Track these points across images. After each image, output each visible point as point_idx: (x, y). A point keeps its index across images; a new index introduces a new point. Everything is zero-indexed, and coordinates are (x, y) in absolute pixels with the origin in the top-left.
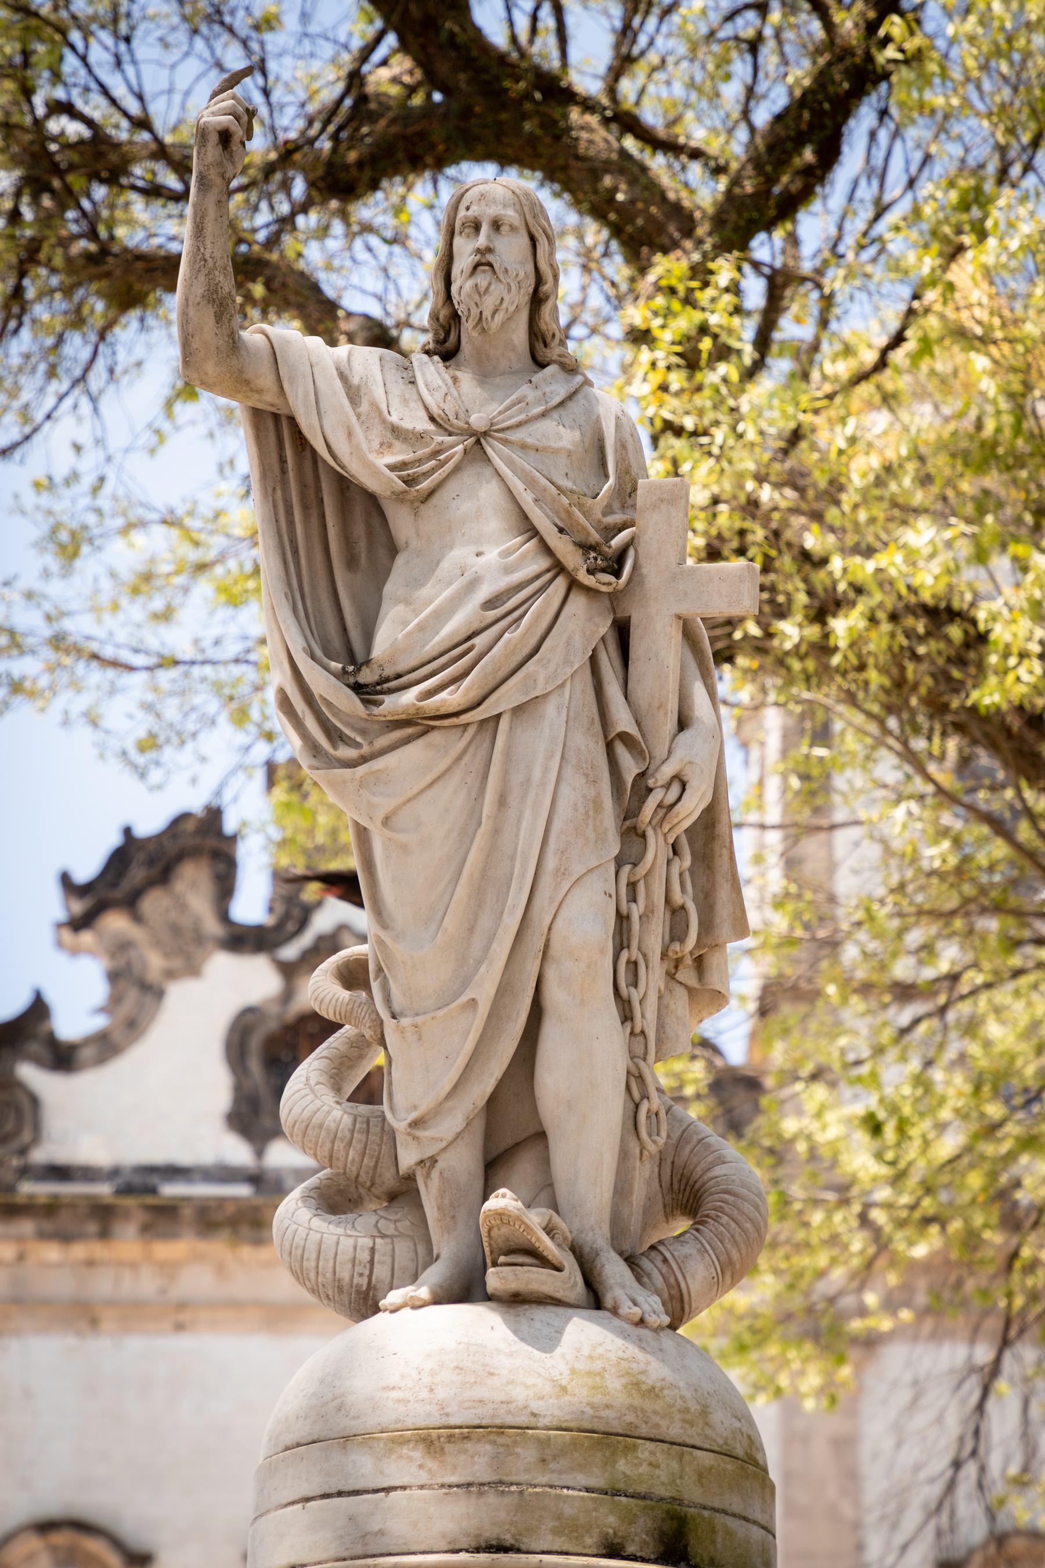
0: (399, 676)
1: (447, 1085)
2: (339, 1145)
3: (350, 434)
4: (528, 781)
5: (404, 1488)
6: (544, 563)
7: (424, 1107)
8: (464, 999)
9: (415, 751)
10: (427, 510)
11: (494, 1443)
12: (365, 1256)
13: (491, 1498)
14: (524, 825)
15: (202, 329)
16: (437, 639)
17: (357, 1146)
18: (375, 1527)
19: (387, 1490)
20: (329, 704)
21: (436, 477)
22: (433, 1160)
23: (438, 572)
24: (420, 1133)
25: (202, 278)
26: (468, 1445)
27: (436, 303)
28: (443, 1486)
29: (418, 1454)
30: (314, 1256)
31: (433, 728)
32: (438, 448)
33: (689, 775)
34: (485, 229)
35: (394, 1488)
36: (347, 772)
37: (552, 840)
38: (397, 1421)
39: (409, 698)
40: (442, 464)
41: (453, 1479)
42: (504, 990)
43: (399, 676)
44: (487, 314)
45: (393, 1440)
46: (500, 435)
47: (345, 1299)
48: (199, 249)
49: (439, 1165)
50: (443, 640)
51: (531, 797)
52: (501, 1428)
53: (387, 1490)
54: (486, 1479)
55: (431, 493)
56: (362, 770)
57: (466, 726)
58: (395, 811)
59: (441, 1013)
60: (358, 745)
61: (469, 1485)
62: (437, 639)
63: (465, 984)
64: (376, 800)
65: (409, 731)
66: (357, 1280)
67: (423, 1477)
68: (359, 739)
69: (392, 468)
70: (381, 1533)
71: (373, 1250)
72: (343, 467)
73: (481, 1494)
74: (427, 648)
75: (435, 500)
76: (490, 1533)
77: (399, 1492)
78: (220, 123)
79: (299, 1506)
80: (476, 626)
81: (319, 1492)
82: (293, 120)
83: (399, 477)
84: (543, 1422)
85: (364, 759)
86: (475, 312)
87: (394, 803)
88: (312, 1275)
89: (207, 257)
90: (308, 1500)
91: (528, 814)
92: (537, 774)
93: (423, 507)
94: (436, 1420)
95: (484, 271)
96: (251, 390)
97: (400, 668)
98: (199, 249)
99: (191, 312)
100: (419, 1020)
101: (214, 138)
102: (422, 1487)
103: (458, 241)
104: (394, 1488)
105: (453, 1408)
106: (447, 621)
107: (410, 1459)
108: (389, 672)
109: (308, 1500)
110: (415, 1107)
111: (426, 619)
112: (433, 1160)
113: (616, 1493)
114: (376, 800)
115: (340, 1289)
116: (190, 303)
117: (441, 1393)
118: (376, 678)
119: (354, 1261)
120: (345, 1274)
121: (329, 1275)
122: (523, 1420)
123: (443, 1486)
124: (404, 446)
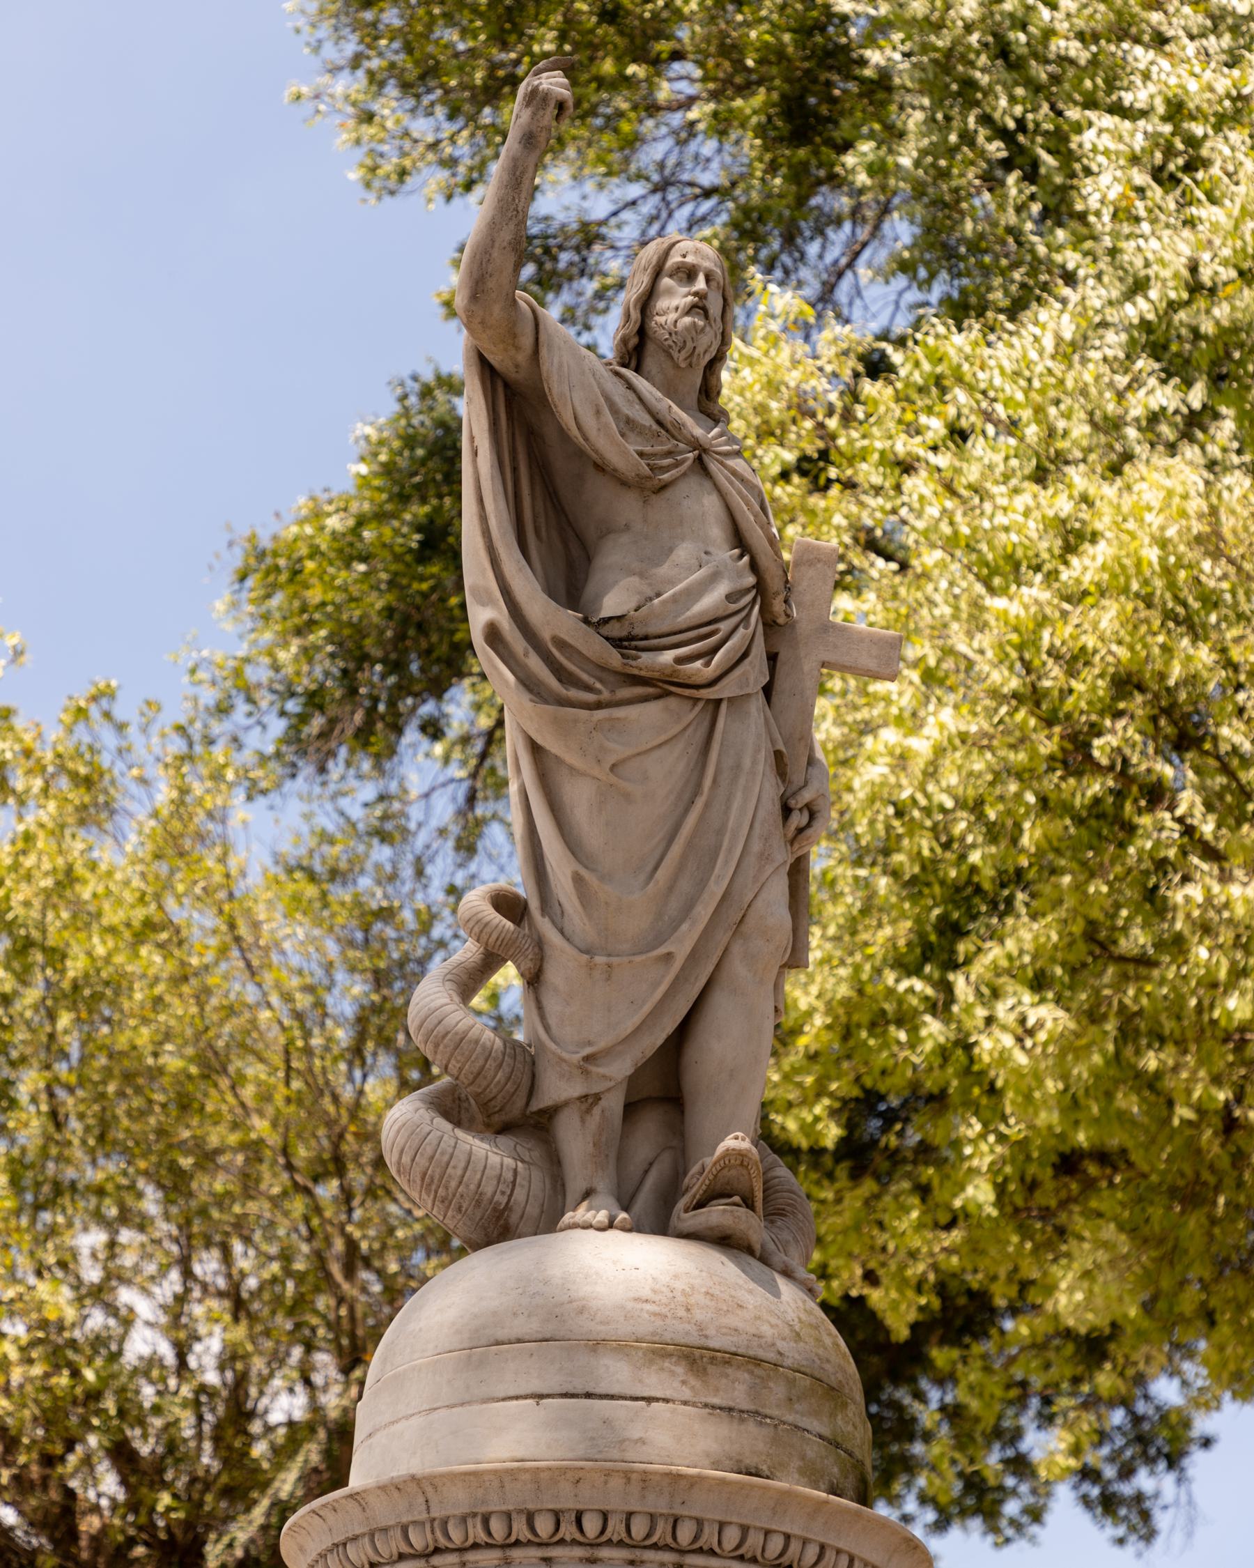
0: (646, 638)
2: (491, 1064)
3: (598, 412)
4: (738, 767)
6: (750, 580)
7: (602, 1044)
8: (662, 950)
9: (652, 712)
10: (658, 501)
11: (751, 1373)
12: (509, 1176)
13: (751, 1426)
14: (736, 805)
17: (506, 1068)
18: (636, 1434)
19: (649, 1400)
20: (561, 644)
22: (597, 1097)
23: (673, 557)
25: (512, 226)
26: (729, 1371)
28: (706, 1406)
31: (670, 694)
35: (657, 1400)
36: (583, 713)
37: (757, 825)
39: (668, 657)
40: (677, 464)
41: (716, 1401)
42: (694, 956)
43: (646, 638)
44: (700, 350)
45: (654, 1352)
47: (478, 1214)
49: (603, 1103)
51: (742, 781)
52: (757, 1361)
53: (649, 1400)
54: (745, 1407)
55: (664, 487)
56: (600, 714)
57: (698, 700)
59: (638, 959)
60: (598, 692)
61: (730, 1409)
63: (660, 940)
64: (611, 745)
65: (650, 690)
66: (498, 1197)
67: (686, 1394)
68: (598, 685)
69: (641, 454)
70: (642, 1441)
71: (515, 1171)
72: (586, 439)
73: (742, 1420)
75: (668, 494)
76: (750, 1461)
77: (661, 1405)
80: (721, 613)
81: (557, 1390)
82: (755, 112)
84: (788, 1362)
85: (599, 706)
86: (690, 345)
87: (629, 752)
88: (453, 1184)
90: (540, 1396)
91: (739, 797)
92: (747, 762)
94: (695, 1339)
97: (653, 629)
101: (552, 104)
102: (685, 1403)
103: (666, 282)
104: (657, 1400)
105: (711, 1332)
106: (696, 601)
107: (673, 1373)
108: (639, 631)
109: (540, 1396)
110: (590, 1043)
111: (681, 593)
112: (597, 1097)
113: (838, 1446)
114: (611, 745)
117: (699, 1315)
118: (624, 633)
120: (488, 1189)
122: (771, 1356)
123: (706, 1406)
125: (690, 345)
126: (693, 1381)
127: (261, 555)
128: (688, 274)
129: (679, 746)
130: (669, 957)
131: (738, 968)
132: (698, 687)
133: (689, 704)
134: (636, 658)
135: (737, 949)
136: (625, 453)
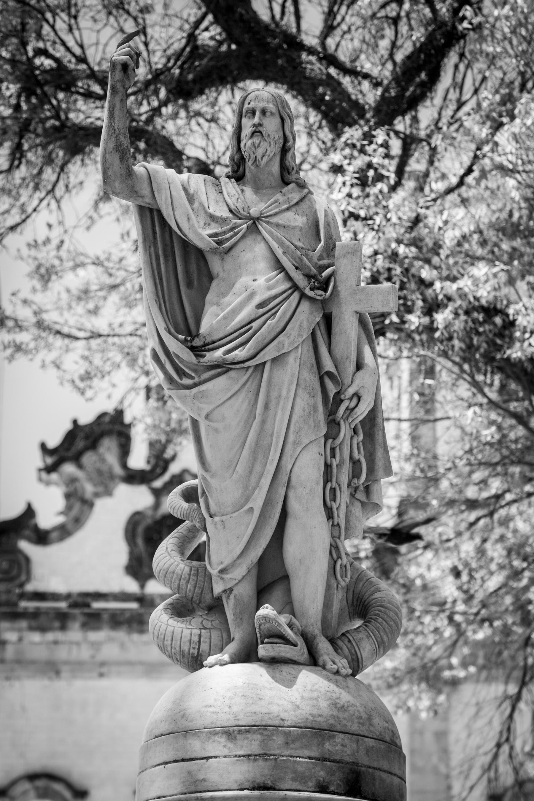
0: (214, 342)
1: (238, 552)
2: (183, 582)
4: (280, 396)
5: (216, 757)
6: (288, 285)
7: (226, 563)
8: (246, 507)
9: (221, 381)
10: (228, 258)
12: (196, 639)
14: (278, 418)
15: (113, 165)
16: (233, 323)
17: (192, 582)
20: (178, 357)
21: (233, 241)
24: (224, 576)
25: (113, 139)
26: (249, 735)
27: (233, 152)
28: (236, 756)
29: (223, 740)
30: (170, 639)
32: (234, 226)
33: (362, 393)
34: (258, 114)
35: (211, 757)
38: (212, 723)
39: (219, 353)
40: (236, 234)
41: (241, 753)
43: (214, 342)
44: (259, 157)
45: (210, 733)
46: (266, 219)
47: (186, 661)
48: (111, 124)
49: (234, 592)
50: (236, 324)
51: (281, 404)
55: (230, 249)
56: (194, 390)
57: (248, 368)
58: (212, 411)
60: (193, 378)
61: (249, 755)
62: (233, 323)
63: (247, 500)
64: (202, 406)
65: (219, 370)
66: (192, 651)
67: (226, 752)
68: (193, 375)
69: (210, 236)
71: (200, 636)
72: (185, 236)
73: (255, 760)
74: (228, 328)
75: (232, 253)
76: (260, 780)
77: (213, 759)
78: (122, 60)
79: (162, 766)
80: (253, 317)
81: (173, 759)
83: (214, 241)
84: (287, 723)
85: (196, 385)
86: (253, 156)
88: (169, 648)
89: (116, 128)
90: (166, 763)
91: (279, 413)
92: (284, 393)
93: (226, 256)
95: (257, 136)
96: (138, 196)
97: (215, 338)
98: (111, 124)
99: (108, 156)
100: (224, 518)
101: (119, 67)
102: (225, 757)
103: (244, 120)
104: (211, 757)
105: (241, 717)
107: (219, 742)
108: (208, 340)
109: (166, 763)
112: (231, 590)
113: (324, 760)
114: (202, 406)
115: (183, 656)
116: (107, 151)
117: (235, 709)
118: (202, 343)
119: (190, 641)
120: (186, 648)
121: (178, 648)
124: (216, 225)
125: (253, 156)
126: (229, 745)
127: (130, 307)
128: (253, 112)
129: (242, 395)
130: (251, 509)
131: (294, 505)
132: (243, 362)
133: (244, 371)
134: (204, 356)
135: (291, 495)
136: (202, 238)
